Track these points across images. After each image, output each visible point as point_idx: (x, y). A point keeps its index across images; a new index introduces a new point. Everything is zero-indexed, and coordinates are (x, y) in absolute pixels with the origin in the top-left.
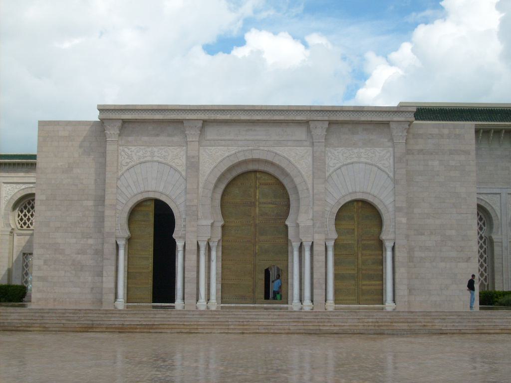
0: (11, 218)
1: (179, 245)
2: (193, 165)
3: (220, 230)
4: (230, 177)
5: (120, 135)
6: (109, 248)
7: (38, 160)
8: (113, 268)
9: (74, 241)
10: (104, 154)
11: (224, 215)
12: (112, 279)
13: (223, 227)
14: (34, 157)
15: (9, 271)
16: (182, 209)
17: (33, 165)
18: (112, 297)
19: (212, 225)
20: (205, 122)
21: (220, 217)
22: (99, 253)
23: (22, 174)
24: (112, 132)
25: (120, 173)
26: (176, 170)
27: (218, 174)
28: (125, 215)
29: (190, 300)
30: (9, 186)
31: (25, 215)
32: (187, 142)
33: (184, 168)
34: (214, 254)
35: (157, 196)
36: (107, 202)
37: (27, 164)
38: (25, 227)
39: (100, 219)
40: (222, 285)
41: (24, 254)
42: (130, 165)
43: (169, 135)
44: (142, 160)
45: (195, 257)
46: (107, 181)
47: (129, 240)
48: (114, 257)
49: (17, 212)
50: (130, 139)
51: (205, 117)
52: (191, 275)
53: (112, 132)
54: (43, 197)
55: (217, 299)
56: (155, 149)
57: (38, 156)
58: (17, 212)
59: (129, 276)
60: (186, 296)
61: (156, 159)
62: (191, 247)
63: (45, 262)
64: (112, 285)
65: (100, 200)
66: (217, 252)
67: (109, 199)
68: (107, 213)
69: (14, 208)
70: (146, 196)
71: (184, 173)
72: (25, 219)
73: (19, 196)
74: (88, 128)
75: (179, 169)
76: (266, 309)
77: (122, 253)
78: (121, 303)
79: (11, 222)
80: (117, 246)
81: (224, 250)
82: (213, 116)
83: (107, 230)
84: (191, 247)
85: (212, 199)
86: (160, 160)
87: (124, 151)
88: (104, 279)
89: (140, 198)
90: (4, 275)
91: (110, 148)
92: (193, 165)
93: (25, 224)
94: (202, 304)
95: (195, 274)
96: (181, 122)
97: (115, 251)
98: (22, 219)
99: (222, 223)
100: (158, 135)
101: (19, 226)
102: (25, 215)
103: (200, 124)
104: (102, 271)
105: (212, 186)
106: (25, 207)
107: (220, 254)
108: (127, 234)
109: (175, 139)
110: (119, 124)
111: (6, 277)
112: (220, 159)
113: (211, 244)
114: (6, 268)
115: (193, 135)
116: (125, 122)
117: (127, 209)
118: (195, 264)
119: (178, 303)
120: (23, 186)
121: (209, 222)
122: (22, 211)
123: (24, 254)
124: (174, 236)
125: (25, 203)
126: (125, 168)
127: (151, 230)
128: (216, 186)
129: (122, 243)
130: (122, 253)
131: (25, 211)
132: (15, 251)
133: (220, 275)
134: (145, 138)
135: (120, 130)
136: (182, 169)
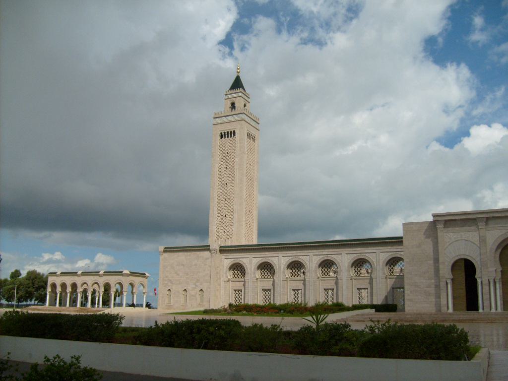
0: (385, 270)
1: (479, 281)
2: (483, 240)
3: (500, 273)
4: (504, 245)
5: (444, 228)
6: (443, 284)
7: (403, 240)
8: (446, 294)
9: (425, 281)
10: (437, 238)
11: (501, 265)
12: (446, 300)
13: (501, 271)
14: (401, 238)
15: (386, 297)
16: (479, 263)
17: (402, 242)
18: (446, 308)
19: (496, 270)
20: (488, 219)
21: (500, 267)
22: (437, 287)
23: (389, 247)
24: (440, 226)
25: (446, 247)
26: (474, 243)
27: (497, 244)
28: (450, 267)
29: (487, 310)
30: (383, 254)
31: (324, 270)
32: (479, 229)
33: (478, 242)
34: (498, 286)
35: (466, 257)
36: (440, 261)
37: (399, 242)
38: (358, 275)
39: (437, 270)
40: (503, 301)
41: (393, 288)
42: (450, 242)
43: (469, 226)
44: (457, 239)
45: (488, 288)
46: (439, 251)
47: (452, 280)
48: (446, 288)
49: (388, 266)
50: (450, 229)
51: (488, 215)
52: (486, 297)
53: (440, 226)
54: (408, 260)
55: (501, 309)
56: (463, 234)
57: (404, 240)
58: (388, 266)
59: (454, 298)
60: (484, 308)
61: (463, 238)
62: (485, 282)
63: (411, 292)
64: (446, 302)
65: (436, 260)
66: (499, 284)
67: (441, 260)
68: (441, 266)
69: (386, 265)
70: (459, 257)
71: (479, 245)
72: (357, 271)
73: (389, 258)
74: (427, 225)
75: (476, 243)
76: (260, 355)
77: (449, 286)
78: (451, 310)
79: (386, 272)
80: (447, 283)
81: (503, 285)
82: (492, 215)
83: (441, 275)
84: (485, 282)
85: (495, 257)
86: (466, 239)
87: (447, 235)
88: (441, 300)
89: (457, 258)
90: (384, 299)
91: (439, 234)
92: (483, 240)
93: (324, 274)
94: (493, 310)
95: (488, 296)
96: (475, 219)
97: (446, 286)
98: (323, 272)
99: (501, 269)
100: (463, 226)
101: (389, 274)
102: (357, 269)
103: (485, 220)
104: (440, 296)
105: (494, 251)
106: (357, 265)
107: (501, 285)
108: (451, 277)
109: (473, 228)
110: (444, 222)
111: (385, 300)
112: (497, 237)
113: (496, 280)
114: (384, 296)
115: (481, 225)
116: (446, 221)
117: (451, 265)
118: (488, 291)
119: (481, 310)
120: (390, 254)
121: (494, 269)
122: (390, 266)
123: (393, 288)
124: (476, 277)
125: (393, 262)
126: (448, 244)
127: (463, 274)
128: (496, 250)
129: (449, 281)
130: (449, 286)
131: (324, 268)
132: (388, 287)
133: (502, 296)
134: (457, 228)
135: (444, 225)
136: (477, 243)
